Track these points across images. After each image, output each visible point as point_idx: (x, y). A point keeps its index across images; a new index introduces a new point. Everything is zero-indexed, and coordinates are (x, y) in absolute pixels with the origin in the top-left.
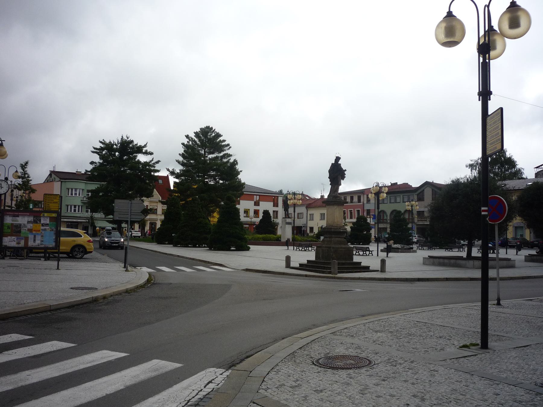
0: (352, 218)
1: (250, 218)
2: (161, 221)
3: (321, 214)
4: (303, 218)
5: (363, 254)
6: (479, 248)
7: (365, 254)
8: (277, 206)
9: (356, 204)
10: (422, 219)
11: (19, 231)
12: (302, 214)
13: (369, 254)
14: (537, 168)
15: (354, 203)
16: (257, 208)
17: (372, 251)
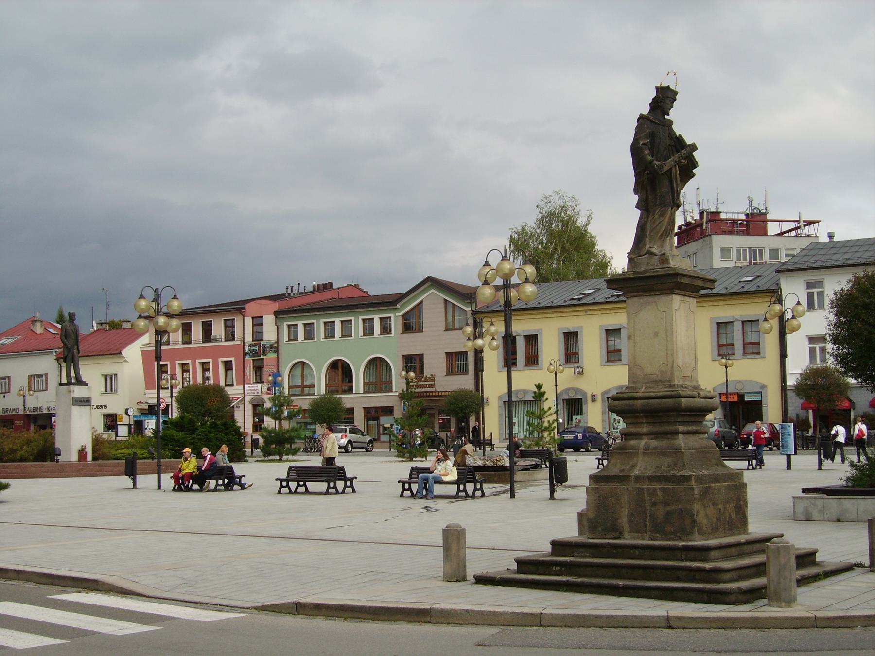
3: (106, 377)
4: (46, 389)
5: (328, 490)
6: (600, 457)
7: (334, 491)
10: (419, 383)
11: (632, 254)
12: (44, 378)
15: (215, 340)
17: (352, 480)
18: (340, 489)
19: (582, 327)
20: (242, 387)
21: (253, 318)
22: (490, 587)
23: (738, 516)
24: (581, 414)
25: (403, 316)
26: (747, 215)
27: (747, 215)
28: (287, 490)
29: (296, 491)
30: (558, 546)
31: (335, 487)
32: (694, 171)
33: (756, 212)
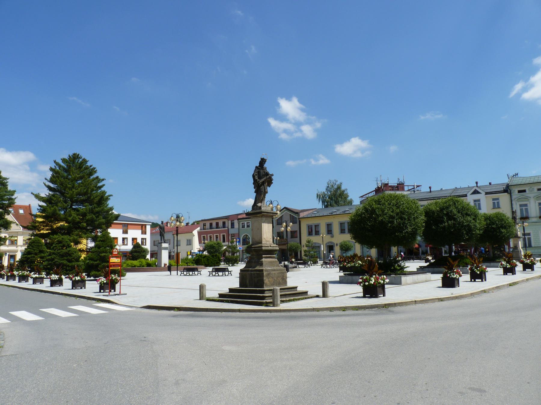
0: (527, 208)
1: (119, 246)
2: (21, 252)
7: (225, 275)
8: (145, 233)
9: (208, 230)
13: (228, 274)
14: (361, 197)
15: (220, 228)
16: (125, 236)
17: (231, 271)
18: (196, 274)
19: (320, 223)
20: (228, 243)
21: (231, 221)
22: (212, 302)
23: (283, 281)
24: (333, 250)
25: (277, 220)
26: (398, 184)
27: (398, 184)
28: (212, 275)
29: (186, 275)
30: (231, 290)
31: (225, 274)
32: (272, 181)
33: (401, 183)
